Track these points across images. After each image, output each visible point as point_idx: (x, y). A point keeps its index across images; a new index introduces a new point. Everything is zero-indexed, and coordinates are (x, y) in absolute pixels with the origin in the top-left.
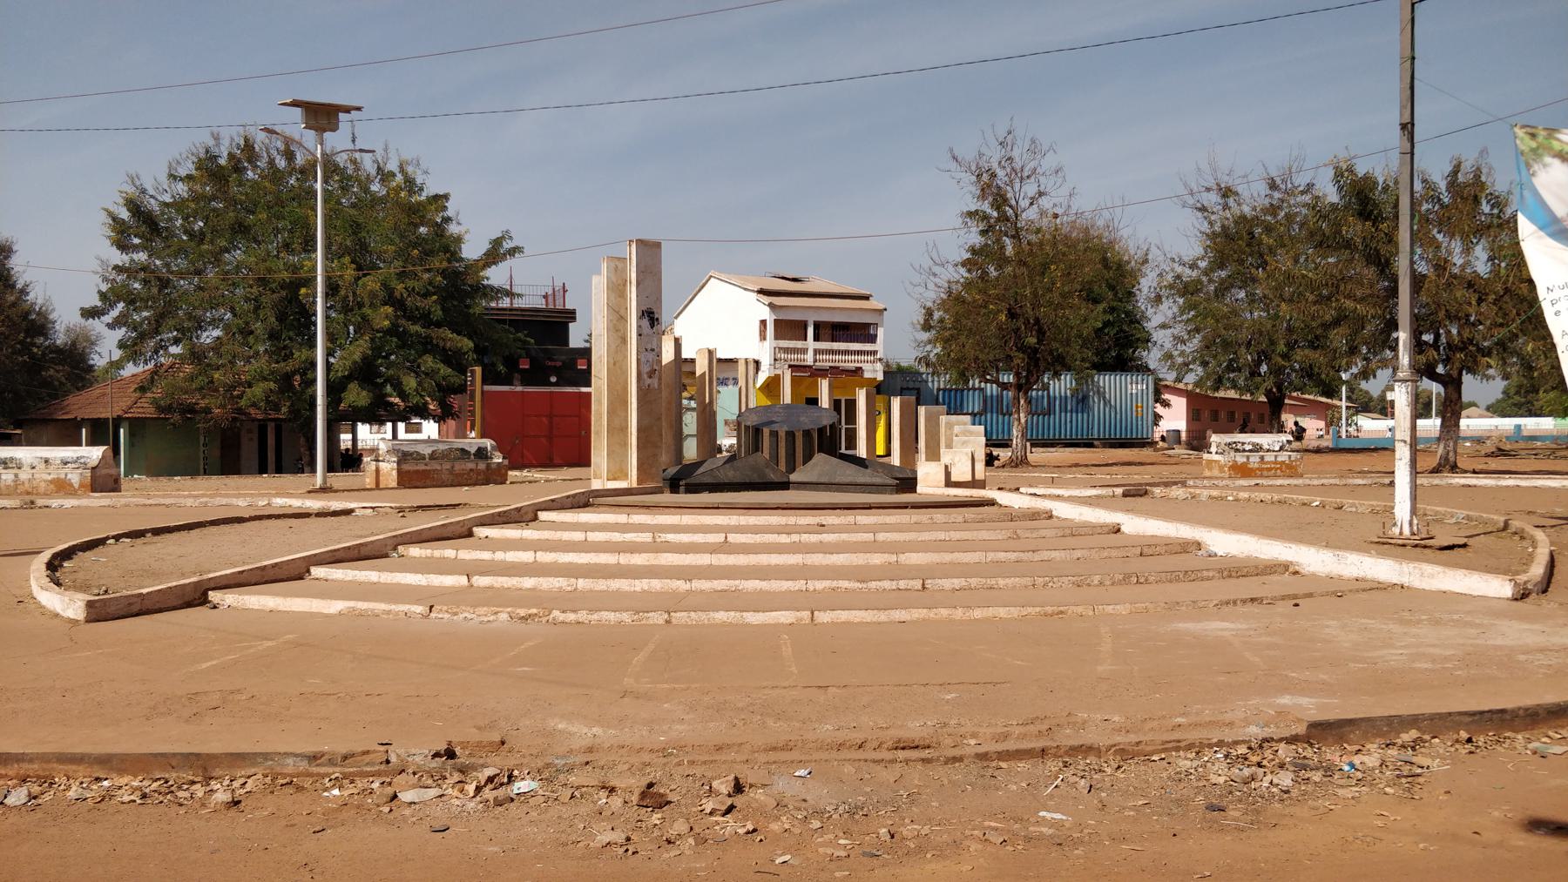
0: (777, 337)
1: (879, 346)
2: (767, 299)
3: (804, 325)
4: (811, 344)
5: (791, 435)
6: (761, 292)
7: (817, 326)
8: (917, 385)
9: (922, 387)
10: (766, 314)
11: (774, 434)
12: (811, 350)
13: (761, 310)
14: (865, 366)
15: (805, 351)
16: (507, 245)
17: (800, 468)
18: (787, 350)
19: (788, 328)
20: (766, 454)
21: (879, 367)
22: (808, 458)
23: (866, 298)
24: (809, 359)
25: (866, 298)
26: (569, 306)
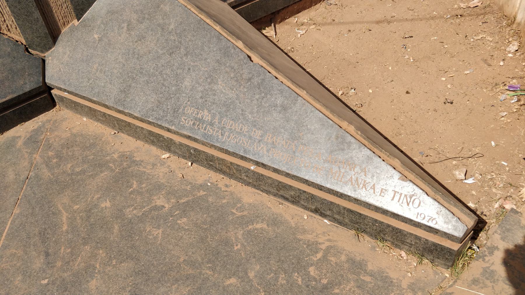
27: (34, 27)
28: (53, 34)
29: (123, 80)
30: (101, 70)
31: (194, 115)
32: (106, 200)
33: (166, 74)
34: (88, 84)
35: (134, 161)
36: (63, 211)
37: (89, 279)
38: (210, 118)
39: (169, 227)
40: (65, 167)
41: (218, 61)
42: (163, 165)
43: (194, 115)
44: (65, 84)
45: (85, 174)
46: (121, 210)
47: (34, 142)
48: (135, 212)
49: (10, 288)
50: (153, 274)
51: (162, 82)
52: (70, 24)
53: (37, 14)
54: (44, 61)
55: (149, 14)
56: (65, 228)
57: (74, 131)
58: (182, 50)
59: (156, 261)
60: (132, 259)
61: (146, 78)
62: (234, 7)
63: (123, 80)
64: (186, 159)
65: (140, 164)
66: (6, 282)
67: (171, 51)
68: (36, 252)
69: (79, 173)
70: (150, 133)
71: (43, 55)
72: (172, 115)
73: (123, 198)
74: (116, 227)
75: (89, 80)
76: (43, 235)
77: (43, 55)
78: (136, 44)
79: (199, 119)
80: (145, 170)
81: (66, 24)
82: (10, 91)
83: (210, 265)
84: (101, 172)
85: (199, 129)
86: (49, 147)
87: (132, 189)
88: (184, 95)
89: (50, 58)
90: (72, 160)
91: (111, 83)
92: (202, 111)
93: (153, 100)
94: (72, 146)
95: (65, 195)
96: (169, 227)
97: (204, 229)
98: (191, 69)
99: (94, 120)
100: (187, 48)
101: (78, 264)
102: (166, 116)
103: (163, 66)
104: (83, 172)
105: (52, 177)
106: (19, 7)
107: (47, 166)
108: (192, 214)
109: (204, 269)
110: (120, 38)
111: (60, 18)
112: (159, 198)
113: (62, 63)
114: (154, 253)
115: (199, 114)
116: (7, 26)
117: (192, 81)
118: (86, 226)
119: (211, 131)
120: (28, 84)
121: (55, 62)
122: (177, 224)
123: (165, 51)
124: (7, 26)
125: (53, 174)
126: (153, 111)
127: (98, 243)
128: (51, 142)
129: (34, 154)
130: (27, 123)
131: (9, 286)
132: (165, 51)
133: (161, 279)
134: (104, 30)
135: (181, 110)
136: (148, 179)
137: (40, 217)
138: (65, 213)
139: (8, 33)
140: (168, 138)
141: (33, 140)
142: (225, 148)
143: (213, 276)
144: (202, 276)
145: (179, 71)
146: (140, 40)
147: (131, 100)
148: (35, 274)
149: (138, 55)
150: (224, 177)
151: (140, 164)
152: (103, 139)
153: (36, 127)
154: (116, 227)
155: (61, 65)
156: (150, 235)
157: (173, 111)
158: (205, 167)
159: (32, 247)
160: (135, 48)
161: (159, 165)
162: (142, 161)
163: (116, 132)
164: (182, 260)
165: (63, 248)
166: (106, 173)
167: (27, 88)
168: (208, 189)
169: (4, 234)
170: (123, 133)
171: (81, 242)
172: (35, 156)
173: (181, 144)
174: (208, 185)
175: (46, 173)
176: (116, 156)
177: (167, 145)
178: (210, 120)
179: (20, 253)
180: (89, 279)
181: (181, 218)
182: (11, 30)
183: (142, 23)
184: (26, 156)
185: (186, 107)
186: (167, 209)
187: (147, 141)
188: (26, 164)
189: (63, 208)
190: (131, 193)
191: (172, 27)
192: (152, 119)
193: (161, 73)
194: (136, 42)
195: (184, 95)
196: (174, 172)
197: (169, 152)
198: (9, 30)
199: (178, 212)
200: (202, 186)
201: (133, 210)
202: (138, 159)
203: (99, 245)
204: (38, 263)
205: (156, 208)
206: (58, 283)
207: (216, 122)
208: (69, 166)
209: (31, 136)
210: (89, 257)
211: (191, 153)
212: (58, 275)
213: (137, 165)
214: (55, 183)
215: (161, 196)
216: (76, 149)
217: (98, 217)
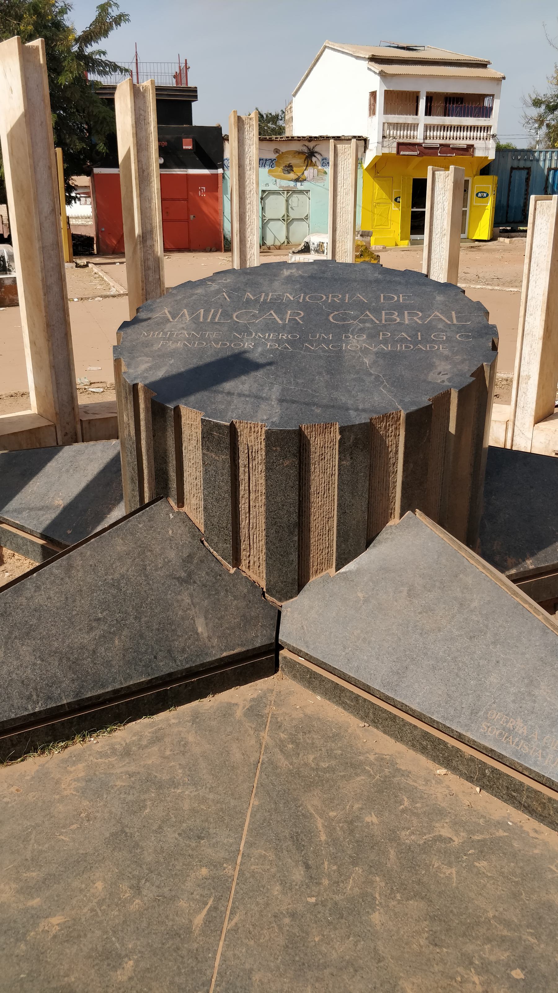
0: (387, 110)
1: (493, 121)
2: (377, 68)
3: (416, 97)
4: (422, 119)
5: (291, 448)
6: (374, 59)
7: (430, 98)
8: (528, 164)
9: (534, 166)
10: (376, 84)
11: (224, 440)
12: (422, 126)
13: (371, 80)
14: (478, 144)
15: (414, 127)
16: (114, 12)
17: (325, 581)
18: (397, 126)
19: (399, 101)
20: (194, 506)
21: (492, 144)
22: (359, 535)
23: (484, 65)
24: (419, 136)
25: (484, 65)
26: (191, 84)
27: (284, 569)
28: (300, 583)
29: (397, 658)
30: (365, 638)
31: (501, 722)
32: (371, 814)
33: (463, 662)
34: (344, 653)
35: (398, 770)
36: (316, 816)
37: (370, 910)
38: (525, 732)
39: (464, 868)
40: (305, 757)
41: (541, 659)
42: (439, 783)
43: (501, 722)
44: (307, 647)
45: (334, 773)
46: (394, 832)
47: (257, 715)
48: (413, 837)
49: (268, 897)
50: (455, 924)
51: (456, 671)
52: (324, 573)
53: (294, 557)
54: (279, 613)
55: (441, 583)
56: (323, 837)
57: (308, 711)
58: (488, 635)
59: (455, 907)
60: (422, 898)
61: (432, 662)
62: (514, 581)
63: (397, 658)
64: (472, 782)
65: (408, 776)
66: (262, 889)
67: (471, 634)
68: (291, 859)
69: (325, 770)
70: (426, 735)
71: (280, 604)
72: (468, 717)
73: (393, 817)
74: (392, 852)
75: (345, 648)
76: (295, 839)
77: (280, 604)
78: (420, 616)
79: (509, 730)
80: (415, 784)
81: (318, 571)
82: (240, 643)
83: (531, 931)
84: (357, 775)
85: (508, 742)
86: (279, 726)
87: (402, 806)
88: (488, 694)
89: (289, 609)
90: (313, 750)
91: (377, 659)
92: (515, 719)
93: (440, 693)
94: (309, 732)
95: (314, 795)
96: (464, 868)
97: (514, 882)
98: (501, 662)
99: (334, 702)
100: (496, 634)
101: (350, 887)
102: (460, 717)
103: (458, 651)
104: (332, 770)
105: (291, 767)
106: (277, 545)
107: (281, 751)
108: (494, 858)
109: (524, 934)
110: (396, 603)
111: (315, 564)
112: (443, 827)
113: (307, 619)
114: (450, 897)
115: (509, 724)
116: (249, 563)
117: (501, 679)
118: (350, 841)
119: (527, 748)
120: (259, 638)
121: (296, 616)
122: (474, 866)
123: (463, 633)
124: (249, 563)
125: (291, 764)
126: (439, 706)
127: (371, 866)
128: (279, 720)
129: (261, 731)
130: (242, 687)
131: (267, 895)
132: (463, 633)
133: (467, 933)
134: (373, 589)
135: (481, 713)
136: (421, 798)
137: (287, 817)
138: (319, 819)
139: (247, 571)
140: (453, 747)
141: (255, 711)
142: (546, 775)
143: (539, 945)
144: (523, 942)
145: (482, 662)
146: (426, 612)
147: (408, 686)
148: (297, 887)
149: (422, 630)
150: (530, 818)
151: (408, 776)
152: (349, 731)
153: (255, 696)
154: (392, 852)
155: (304, 621)
156: (441, 873)
157: (469, 711)
158: (501, 798)
159: (285, 853)
160: (418, 621)
161: (434, 782)
162: (410, 772)
163: (367, 725)
164: (491, 915)
165: (326, 863)
166: (363, 778)
167: (258, 643)
168: (509, 829)
169: (246, 828)
170: (377, 728)
171: (349, 860)
172: (262, 734)
173: (472, 759)
174: (508, 824)
175: (283, 762)
176: (372, 757)
177: (447, 757)
178: (525, 734)
179: (271, 856)
180: (370, 910)
181: (479, 860)
182: (251, 567)
183: (429, 591)
184: (252, 732)
185: (489, 710)
186: (456, 843)
187: (413, 746)
188: (253, 742)
189: (314, 811)
190: (403, 811)
191: (475, 604)
192: (438, 717)
193: (455, 659)
194: (420, 613)
195: (488, 694)
196: (457, 796)
197: (446, 768)
198: (249, 567)
199: (473, 851)
200: (500, 824)
201: (410, 835)
202: (403, 768)
203: (373, 870)
204: (298, 874)
205: (440, 839)
206: (329, 905)
207: (534, 738)
208: (311, 757)
209: (251, 707)
210: (364, 883)
211: (484, 775)
212: (328, 895)
213: (403, 775)
214: (297, 776)
215: (445, 825)
216: (315, 737)
217: (365, 834)
